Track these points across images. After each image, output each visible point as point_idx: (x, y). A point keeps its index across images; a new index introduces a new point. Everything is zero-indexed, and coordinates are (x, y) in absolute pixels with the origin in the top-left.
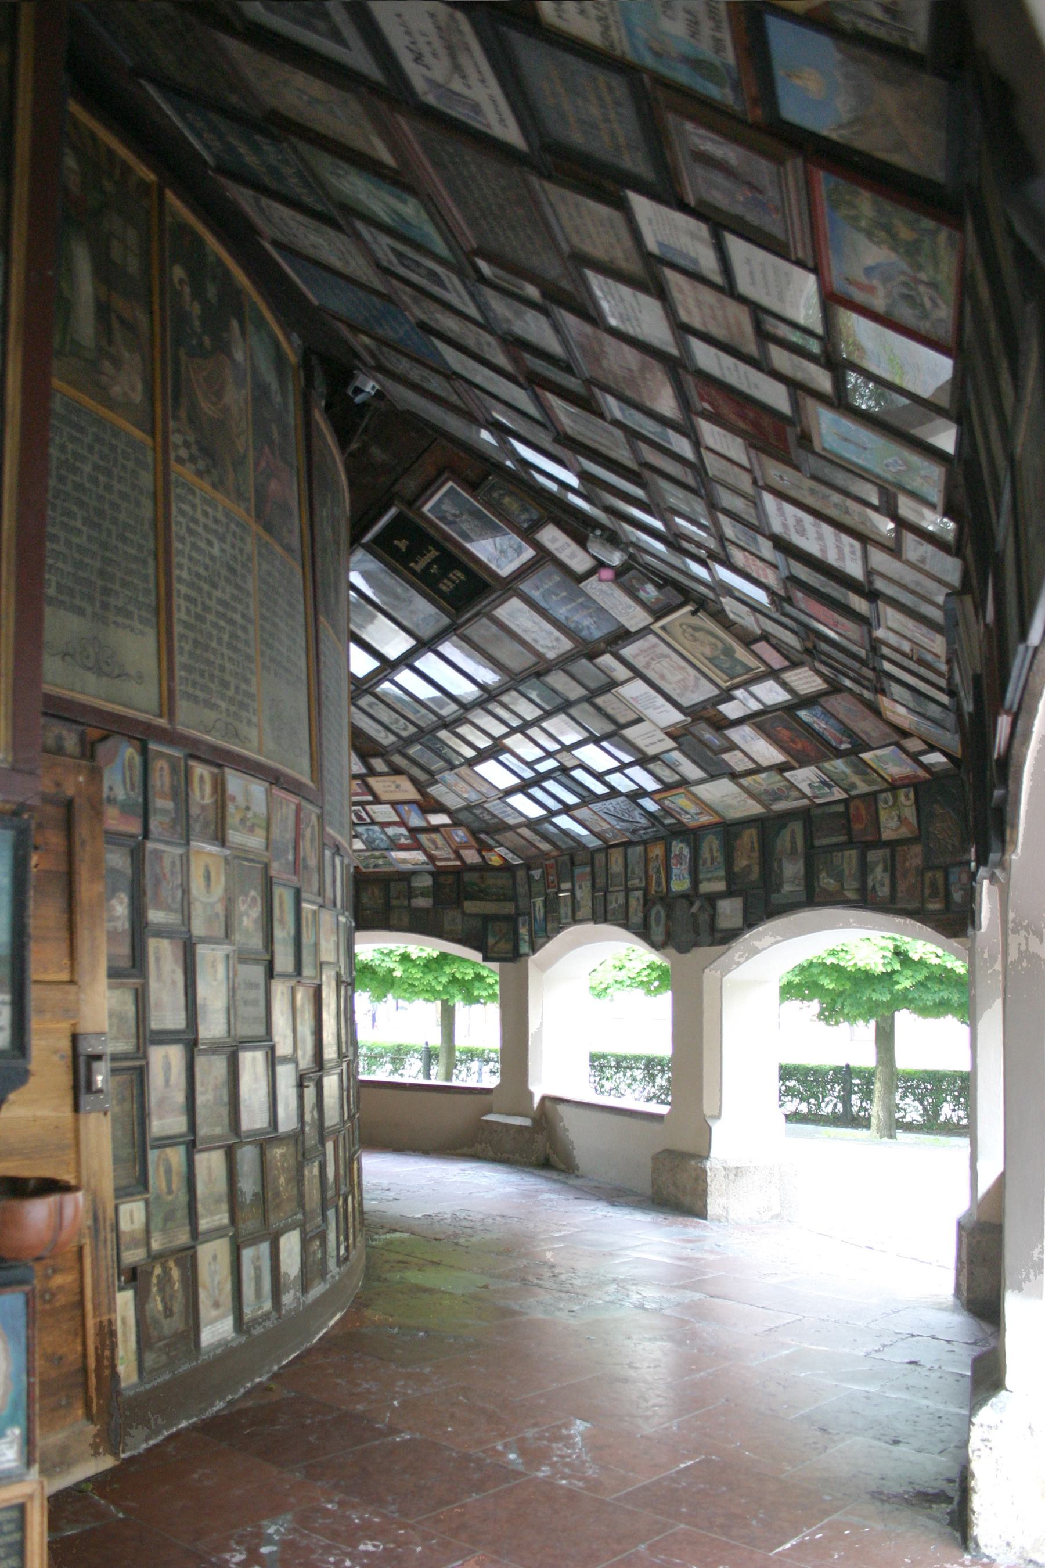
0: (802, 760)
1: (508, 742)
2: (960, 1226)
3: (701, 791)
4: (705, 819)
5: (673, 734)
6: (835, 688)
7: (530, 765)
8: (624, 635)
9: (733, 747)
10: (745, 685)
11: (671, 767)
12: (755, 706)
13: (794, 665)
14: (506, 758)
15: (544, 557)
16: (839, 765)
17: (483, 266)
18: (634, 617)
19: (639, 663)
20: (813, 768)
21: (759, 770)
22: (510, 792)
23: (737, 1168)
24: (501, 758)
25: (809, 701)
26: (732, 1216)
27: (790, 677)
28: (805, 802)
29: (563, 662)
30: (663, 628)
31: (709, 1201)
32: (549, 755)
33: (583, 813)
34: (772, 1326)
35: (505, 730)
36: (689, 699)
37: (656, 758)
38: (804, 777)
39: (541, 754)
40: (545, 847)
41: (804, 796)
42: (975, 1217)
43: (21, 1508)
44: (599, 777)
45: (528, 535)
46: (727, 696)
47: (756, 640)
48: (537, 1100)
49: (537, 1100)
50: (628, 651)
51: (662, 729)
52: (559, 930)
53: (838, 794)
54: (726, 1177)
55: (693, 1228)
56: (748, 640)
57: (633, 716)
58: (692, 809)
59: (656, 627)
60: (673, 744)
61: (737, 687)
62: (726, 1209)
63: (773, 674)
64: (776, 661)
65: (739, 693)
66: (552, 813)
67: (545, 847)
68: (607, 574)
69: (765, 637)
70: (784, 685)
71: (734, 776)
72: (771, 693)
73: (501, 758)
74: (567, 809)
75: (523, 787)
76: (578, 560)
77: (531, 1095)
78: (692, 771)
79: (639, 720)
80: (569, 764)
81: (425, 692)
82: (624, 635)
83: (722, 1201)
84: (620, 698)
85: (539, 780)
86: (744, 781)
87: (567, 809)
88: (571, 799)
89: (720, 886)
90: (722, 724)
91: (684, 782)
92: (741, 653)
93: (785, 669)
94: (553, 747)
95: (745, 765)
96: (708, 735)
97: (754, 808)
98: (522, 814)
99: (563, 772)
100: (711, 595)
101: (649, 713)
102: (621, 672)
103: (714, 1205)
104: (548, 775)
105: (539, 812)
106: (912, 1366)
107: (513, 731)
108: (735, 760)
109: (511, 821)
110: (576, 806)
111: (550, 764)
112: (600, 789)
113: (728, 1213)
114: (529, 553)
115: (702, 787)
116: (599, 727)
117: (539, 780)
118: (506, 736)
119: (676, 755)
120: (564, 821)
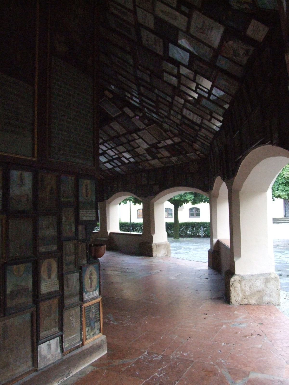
0: (173, 155)
1: (107, 152)
2: (209, 251)
3: (150, 162)
4: (150, 168)
5: (146, 150)
6: (183, 141)
7: (111, 157)
8: (139, 130)
9: (159, 153)
10: (164, 140)
11: (145, 157)
12: (165, 144)
13: (175, 136)
14: (106, 155)
15: (124, 113)
16: (181, 157)
17: (140, 67)
18: (142, 126)
19: (141, 135)
20: (176, 157)
21: (164, 157)
22: (105, 163)
23: (158, 245)
24: (105, 155)
25: (178, 144)
26: (158, 256)
27: (174, 139)
28: (173, 164)
29: (124, 135)
30: (148, 129)
31: (153, 253)
32: (116, 154)
33: (122, 167)
34: (178, 275)
35: (107, 149)
36: (151, 143)
37: (141, 155)
38: (174, 159)
39: (115, 154)
40: (111, 174)
41: (173, 163)
42: (213, 249)
43: (99, 302)
44: (127, 159)
45: (121, 109)
46: (159, 142)
47: (168, 131)
48: (109, 233)
49: (109, 233)
50: (139, 133)
51: (144, 149)
52: (114, 194)
53: (181, 162)
54: (156, 247)
55: (151, 259)
56: (166, 131)
57: (137, 146)
58: (148, 166)
59: (146, 128)
60: (146, 152)
61: (163, 140)
62: (156, 254)
63: (170, 138)
64: (171, 135)
65: (162, 142)
66: (114, 167)
67: (111, 174)
68: (137, 117)
69: (170, 131)
70: (172, 140)
71: (159, 159)
72: (169, 142)
73: (105, 155)
74: (118, 166)
75: (108, 162)
76: (131, 114)
77: (108, 232)
78: (149, 158)
79: (139, 147)
80: (121, 156)
81: (111, 145)
82: (139, 130)
83: (156, 253)
84: (135, 142)
85: (113, 160)
86: (160, 160)
87: (118, 166)
88: (119, 164)
89: (154, 183)
90: (157, 148)
91: (147, 160)
92: (164, 134)
93: (173, 137)
94: (117, 153)
95: (162, 156)
96: (154, 150)
97: (162, 165)
98: (107, 167)
99: (119, 159)
100: (160, 123)
101: (141, 145)
102: (137, 137)
103: (154, 254)
104: (115, 159)
105: (111, 167)
106: (207, 279)
107: (109, 149)
108: (159, 155)
109: (104, 169)
110: (121, 166)
111: (117, 156)
112: (127, 161)
113: (157, 255)
114: (120, 112)
115: (151, 161)
116: (130, 148)
117: (113, 160)
118: (107, 150)
119: (147, 155)
120: (118, 169)
